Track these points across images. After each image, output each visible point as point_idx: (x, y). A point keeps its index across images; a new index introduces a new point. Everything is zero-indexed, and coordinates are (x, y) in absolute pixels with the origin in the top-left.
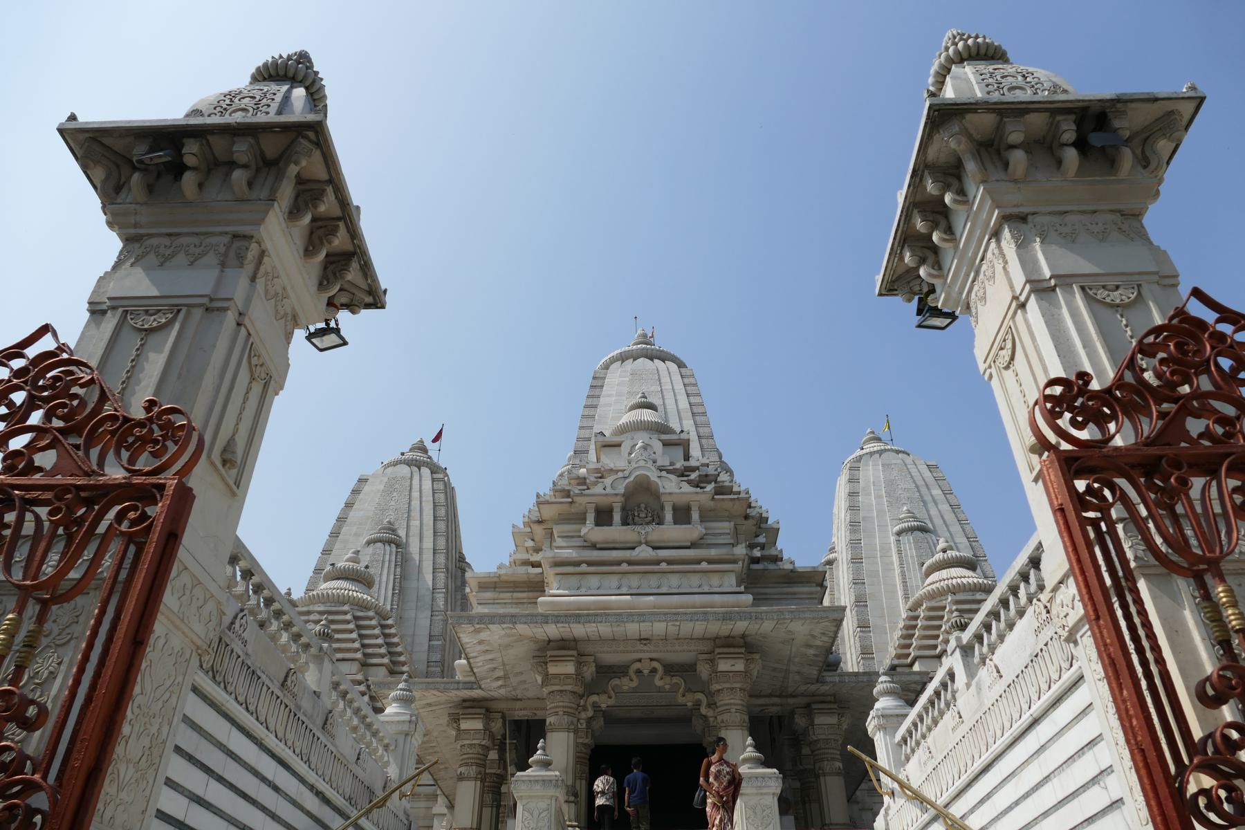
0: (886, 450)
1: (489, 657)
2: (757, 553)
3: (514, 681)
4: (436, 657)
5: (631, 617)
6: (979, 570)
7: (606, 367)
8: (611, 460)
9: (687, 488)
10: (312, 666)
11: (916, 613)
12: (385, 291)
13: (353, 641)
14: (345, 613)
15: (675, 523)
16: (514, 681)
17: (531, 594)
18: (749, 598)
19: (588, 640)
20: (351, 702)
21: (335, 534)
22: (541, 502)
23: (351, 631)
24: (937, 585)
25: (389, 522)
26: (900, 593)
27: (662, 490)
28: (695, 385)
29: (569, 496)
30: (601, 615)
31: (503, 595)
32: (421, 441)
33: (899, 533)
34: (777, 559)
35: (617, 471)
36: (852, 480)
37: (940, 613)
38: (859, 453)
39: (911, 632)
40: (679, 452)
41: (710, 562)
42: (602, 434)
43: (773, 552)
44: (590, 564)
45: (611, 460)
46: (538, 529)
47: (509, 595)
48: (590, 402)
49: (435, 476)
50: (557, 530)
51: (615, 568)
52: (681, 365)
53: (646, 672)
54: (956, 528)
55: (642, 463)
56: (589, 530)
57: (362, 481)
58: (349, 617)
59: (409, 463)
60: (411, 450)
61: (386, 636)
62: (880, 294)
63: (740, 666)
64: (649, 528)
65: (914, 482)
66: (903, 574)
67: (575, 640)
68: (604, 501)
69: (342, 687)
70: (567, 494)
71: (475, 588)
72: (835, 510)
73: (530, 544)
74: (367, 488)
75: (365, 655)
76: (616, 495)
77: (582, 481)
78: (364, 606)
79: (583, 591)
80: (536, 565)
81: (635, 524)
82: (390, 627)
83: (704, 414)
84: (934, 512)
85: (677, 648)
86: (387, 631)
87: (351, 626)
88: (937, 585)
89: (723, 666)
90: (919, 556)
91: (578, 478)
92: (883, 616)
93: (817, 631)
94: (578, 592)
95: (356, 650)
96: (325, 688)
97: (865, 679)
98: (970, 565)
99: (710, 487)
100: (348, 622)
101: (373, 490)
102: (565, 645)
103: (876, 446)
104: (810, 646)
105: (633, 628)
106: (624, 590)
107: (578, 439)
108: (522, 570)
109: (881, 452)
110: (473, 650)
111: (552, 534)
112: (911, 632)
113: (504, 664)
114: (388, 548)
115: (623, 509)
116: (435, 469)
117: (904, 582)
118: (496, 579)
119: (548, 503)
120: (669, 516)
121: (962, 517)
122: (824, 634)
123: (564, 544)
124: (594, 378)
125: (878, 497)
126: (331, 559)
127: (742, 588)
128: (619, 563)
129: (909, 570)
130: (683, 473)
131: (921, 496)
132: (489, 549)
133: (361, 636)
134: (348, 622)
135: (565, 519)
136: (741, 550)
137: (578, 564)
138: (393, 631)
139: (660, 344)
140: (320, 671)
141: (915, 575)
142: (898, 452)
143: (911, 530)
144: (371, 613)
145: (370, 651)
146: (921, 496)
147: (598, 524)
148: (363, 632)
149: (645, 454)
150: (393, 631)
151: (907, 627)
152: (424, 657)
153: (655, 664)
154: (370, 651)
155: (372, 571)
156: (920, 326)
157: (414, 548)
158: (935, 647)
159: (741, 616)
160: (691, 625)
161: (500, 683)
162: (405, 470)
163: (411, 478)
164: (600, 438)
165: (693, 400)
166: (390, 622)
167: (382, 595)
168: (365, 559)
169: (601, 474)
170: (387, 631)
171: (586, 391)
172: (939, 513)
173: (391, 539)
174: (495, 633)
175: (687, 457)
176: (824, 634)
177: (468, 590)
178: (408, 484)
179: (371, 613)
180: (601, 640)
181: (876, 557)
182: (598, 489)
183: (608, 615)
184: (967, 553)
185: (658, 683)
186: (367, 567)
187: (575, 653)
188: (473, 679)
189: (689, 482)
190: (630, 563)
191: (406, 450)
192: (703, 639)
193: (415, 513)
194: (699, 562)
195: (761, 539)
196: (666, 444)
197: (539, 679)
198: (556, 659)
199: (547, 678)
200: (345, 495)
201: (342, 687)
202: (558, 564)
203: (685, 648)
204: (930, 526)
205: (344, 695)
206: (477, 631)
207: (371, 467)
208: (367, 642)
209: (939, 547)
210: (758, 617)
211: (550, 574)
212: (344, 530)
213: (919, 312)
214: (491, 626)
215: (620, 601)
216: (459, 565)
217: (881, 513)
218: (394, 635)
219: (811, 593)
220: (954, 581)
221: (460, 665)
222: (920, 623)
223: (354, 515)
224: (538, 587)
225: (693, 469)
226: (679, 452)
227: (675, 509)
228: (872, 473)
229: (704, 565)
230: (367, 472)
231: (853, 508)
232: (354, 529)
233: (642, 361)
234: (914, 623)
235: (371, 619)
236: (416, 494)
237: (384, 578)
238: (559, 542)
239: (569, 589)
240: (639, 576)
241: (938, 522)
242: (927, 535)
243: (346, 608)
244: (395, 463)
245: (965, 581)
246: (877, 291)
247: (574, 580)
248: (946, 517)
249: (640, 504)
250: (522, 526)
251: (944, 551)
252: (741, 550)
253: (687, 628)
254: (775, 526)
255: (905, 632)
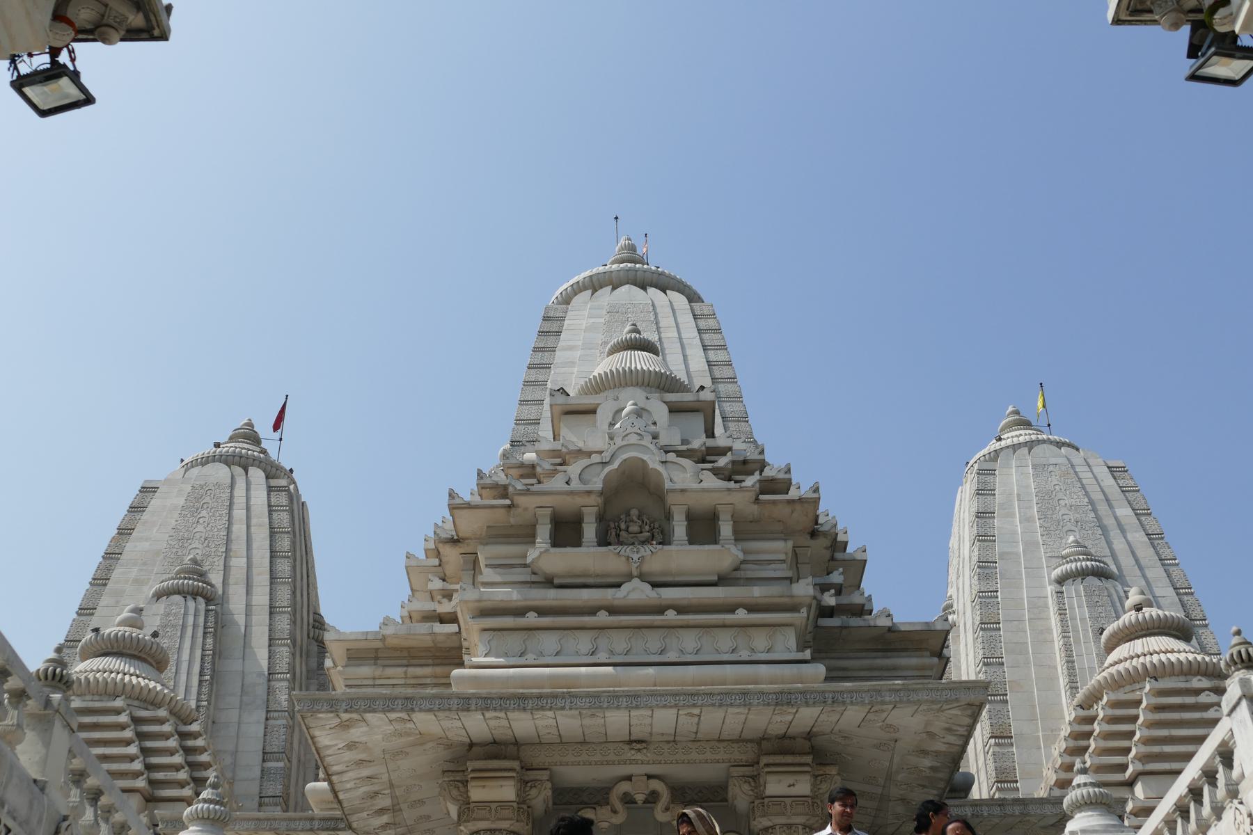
0: (1039, 442)
1: (365, 772)
2: (830, 600)
3: (409, 815)
4: (274, 788)
5: (615, 699)
6: (1194, 641)
7: (566, 300)
8: (577, 436)
9: (711, 481)
10: (30, 736)
11: (1091, 712)
12: (169, 8)
13: (132, 759)
14: (118, 712)
15: (691, 542)
16: (409, 815)
17: (439, 670)
18: (820, 669)
19: (538, 743)
20: (109, 811)
21: (100, 581)
22: (456, 506)
23: (128, 743)
24: (1127, 664)
25: (194, 561)
26: (1062, 681)
27: (668, 485)
28: (717, 331)
29: (505, 496)
30: (563, 696)
31: (390, 671)
32: (250, 424)
33: (1061, 581)
34: (862, 610)
35: (589, 454)
36: (983, 491)
37: (1132, 712)
38: (994, 445)
39: (1083, 743)
40: (698, 422)
41: (751, 609)
42: (562, 391)
43: (856, 599)
44: (542, 612)
45: (577, 436)
46: (452, 555)
47: (400, 671)
48: (539, 358)
49: (273, 482)
50: (484, 554)
51: (587, 620)
52: (693, 297)
53: (640, 798)
54: (1155, 572)
55: (633, 439)
56: (541, 554)
57: (148, 490)
58: (123, 718)
59: (228, 460)
60: (232, 439)
61: (188, 751)
62: (1117, 21)
63: (803, 787)
64: (645, 551)
65: (1087, 494)
66: (1067, 648)
67: (516, 743)
68: (567, 504)
69: (91, 782)
70: (503, 491)
71: (342, 661)
72: (953, 543)
73: (437, 584)
74: (155, 503)
75: (151, 782)
76: (589, 492)
77: (529, 471)
78: (152, 701)
79: (530, 658)
80: (452, 619)
81: (621, 543)
82: (194, 736)
83: (732, 380)
84: (1119, 545)
85: (694, 756)
86: (190, 743)
87: (128, 734)
88: (1127, 664)
89: (775, 786)
90: (1095, 619)
91: (522, 465)
92: (1033, 719)
93: (938, 726)
94: (522, 661)
95: (136, 775)
96: (57, 778)
97: (1017, 810)
98: (1182, 631)
99: (750, 481)
100: (122, 727)
101: (165, 507)
102: (499, 752)
103: (1023, 435)
104: (924, 753)
105: (617, 721)
106: (602, 657)
107: (519, 421)
108: (423, 628)
109: (1030, 445)
110: (338, 759)
111: (475, 562)
112: (1083, 743)
113: (392, 786)
114: (191, 604)
115: (601, 518)
116: (273, 471)
117: (1070, 663)
118: (379, 645)
119: (469, 506)
120: (680, 529)
121: (1166, 553)
122: (949, 730)
123: (498, 579)
124: (546, 318)
125: (1026, 520)
126: (95, 622)
127: (807, 654)
128: (593, 611)
129: (1077, 641)
130: (704, 457)
131: (1098, 518)
132: (362, 595)
133: (145, 752)
134: (122, 727)
135: (498, 535)
136: (804, 589)
137: (520, 612)
138: (200, 742)
139: (659, 261)
140: (47, 744)
141: (1088, 650)
142: (1059, 445)
143: (1082, 574)
144: (162, 713)
145: (160, 776)
146: (1098, 518)
147: (555, 544)
148: (149, 744)
149: (640, 423)
150: (200, 742)
151: (1075, 736)
152: (254, 788)
153: (656, 785)
154: (160, 776)
155: (164, 642)
156: (1194, 77)
157: (236, 604)
158: (1123, 768)
159: (807, 697)
160: (718, 714)
161: (385, 819)
162: (220, 472)
163: (232, 486)
164: (560, 399)
165: (712, 355)
166: (195, 727)
167: (182, 682)
168: (152, 622)
169: (562, 459)
170: (190, 743)
171: (532, 339)
172: (1128, 548)
173: (196, 589)
174: (377, 730)
175: (710, 434)
176: (949, 730)
177: (328, 663)
178: (226, 495)
179: (162, 713)
180: (562, 743)
181: (1021, 620)
182: (557, 483)
183: (575, 696)
184: (1177, 613)
185: (661, 816)
186: (155, 635)
187: (515, 764)
188: (338, 813)
189: (716, 472)
190: (613, 610)
191: (223, 438)
192: (740, 740)
193: (239, 546)
194: (731, 609)
195: (837, 578)
196: (675, 409)
197: (453, 810)
198: (484, 776)
199: (467, 809)
200: (119, 513)
201: (91, 782)
202: (485, 613)
203: (709, 756)
204: (1113, 568)
205: (95, 796)
206: (345, 726)
207: (163, 468)
208: (155, 760)
209: (1128, 604)
210: (837, 700)
211: (471, 629)
212: (116, 574)
213: (1193, 52)
214: (368, 716)
215: (595, 676)
216: (310, 633)
217: (1030, 545)
218: (202, 750)
219: (923, 668)
220: (1155, 658)
221: (314, 791)
222: (1097, 727)
223: (132, 548)
224: (453, 655)
225: (723, 451)
226: (698, 422)
227: (691, 518)
228: (1015, 479)
229: (741, 615)
230: (156, 474)
231: (984, 538)
232: (134, 572)
233: (628, 293)
234: (1087, 728)
235: (161, 721)
236: (239, 513)
237: (185, 656)
238: (488, 574)
239: (506, 655)
240: (628, 633)
241: (1127, 561)
242: (1109, 584)
243: (119, 703)
244: (205, 461)
245: (1173, 657)
246: (1110, 15)
247: (514, 641)
248: (1140, 554)
249: (631, 509)
250: (422, 556)
251: (1138, 608)
252: (804, 589)
253: (714, 720)
254: (859, 556)
255: (1072, 743)
